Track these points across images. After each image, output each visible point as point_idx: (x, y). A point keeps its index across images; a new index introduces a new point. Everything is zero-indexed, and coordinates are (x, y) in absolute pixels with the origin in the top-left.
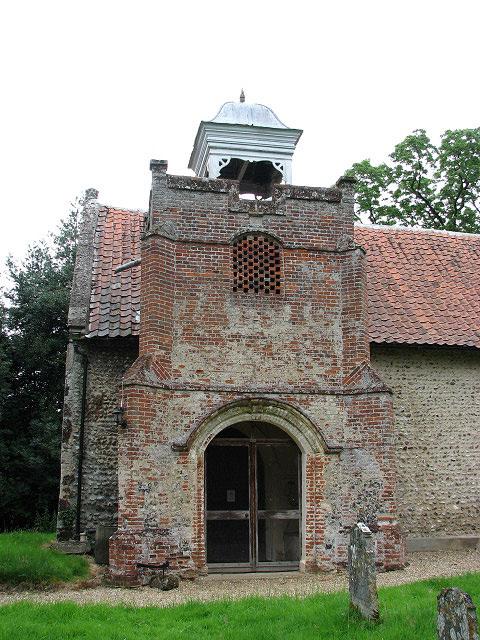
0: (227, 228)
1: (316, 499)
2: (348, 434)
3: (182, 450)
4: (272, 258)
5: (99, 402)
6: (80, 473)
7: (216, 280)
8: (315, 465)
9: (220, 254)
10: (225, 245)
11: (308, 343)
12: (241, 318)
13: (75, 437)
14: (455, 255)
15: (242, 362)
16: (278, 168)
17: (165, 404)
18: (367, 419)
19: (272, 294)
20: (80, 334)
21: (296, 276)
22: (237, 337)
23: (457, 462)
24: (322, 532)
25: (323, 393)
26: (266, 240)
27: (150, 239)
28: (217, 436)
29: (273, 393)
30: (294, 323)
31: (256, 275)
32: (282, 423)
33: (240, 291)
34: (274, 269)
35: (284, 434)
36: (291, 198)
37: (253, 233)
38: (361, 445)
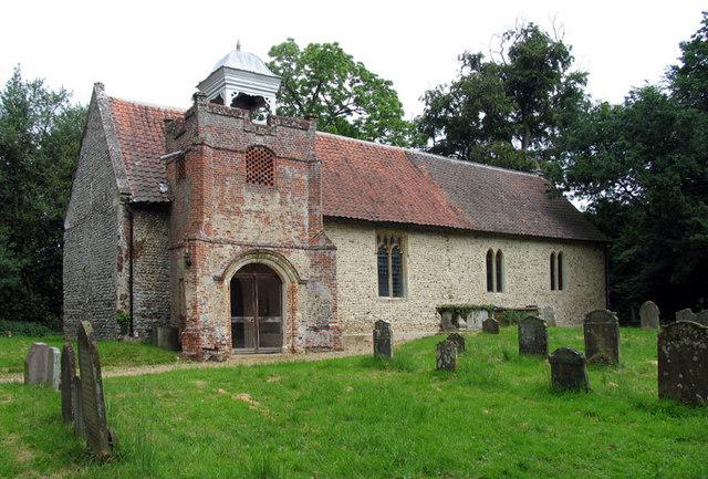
1: (293, 310)
2: (311, 273)
3: (220, 280)
6: (131, 292)
8: (293, 291)
12: (252, 199)
21: (285, 176)
22: (249, 211)
35: (266, 266)
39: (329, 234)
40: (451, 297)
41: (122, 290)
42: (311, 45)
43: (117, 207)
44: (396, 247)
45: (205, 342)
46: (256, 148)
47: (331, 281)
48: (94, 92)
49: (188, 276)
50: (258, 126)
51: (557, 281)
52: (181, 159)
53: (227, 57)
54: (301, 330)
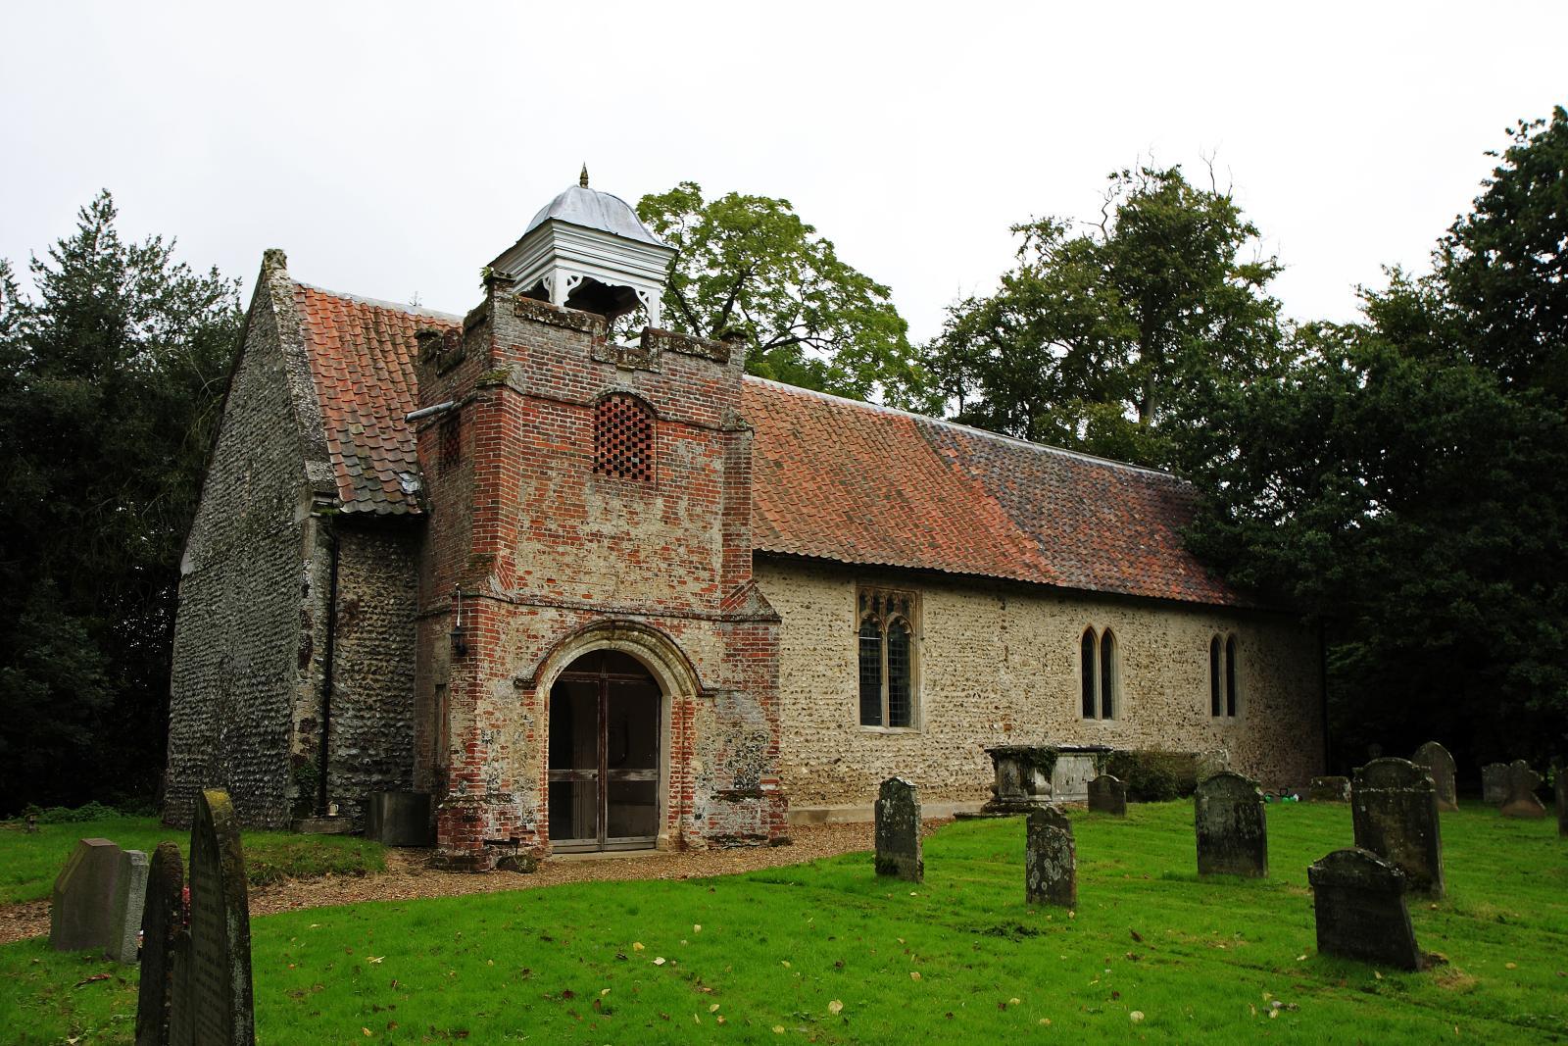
0: (589, 384)
1: (684, 755)
2: (725, 672)
3: (527, 686)
4: (641, 431)
5: (353, 608)
6: (326, 713)
7: (573, 455)
8: (685, 711)
9: (579, 419)
10: (585, 406)
11: (682, 550)
13: (317, 661)
14: (795, 421)
15: (603, 571)
16: (642, 299)
17: (508, 623)
18: (751, 655)
19: (641, 480)
20: (331, 506)
21: (672, 459)
22: (596, 536)
23: (809, 712)
24: (690, 798)
25: (698, 617)
26: (635, 405)
27: (494, 390)
28: (566, 669)
29: (640, 614)
30: (666, 523)
31: (622, 453)
32: (646, 654)
33: (602, 474)
34: (643, 446)
36: (669, 350)
37: (621, 394)
38: (743, 686)
39: (763, 587)
40: (1008, 728)
41: (304, 709)
42: (734, 195)
43: (304, 525)
44: (897, 620)
45: (491, 827)
46: (616, 400)
47: (767, 693)
48: (263, 271)
49: (458, 678)
50: (621, 352)
51: (1224, 699)
52: (450, 422)
53: (557, 203)
54: (701, 799)
